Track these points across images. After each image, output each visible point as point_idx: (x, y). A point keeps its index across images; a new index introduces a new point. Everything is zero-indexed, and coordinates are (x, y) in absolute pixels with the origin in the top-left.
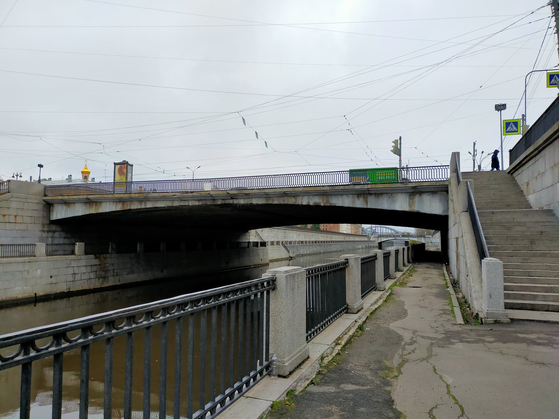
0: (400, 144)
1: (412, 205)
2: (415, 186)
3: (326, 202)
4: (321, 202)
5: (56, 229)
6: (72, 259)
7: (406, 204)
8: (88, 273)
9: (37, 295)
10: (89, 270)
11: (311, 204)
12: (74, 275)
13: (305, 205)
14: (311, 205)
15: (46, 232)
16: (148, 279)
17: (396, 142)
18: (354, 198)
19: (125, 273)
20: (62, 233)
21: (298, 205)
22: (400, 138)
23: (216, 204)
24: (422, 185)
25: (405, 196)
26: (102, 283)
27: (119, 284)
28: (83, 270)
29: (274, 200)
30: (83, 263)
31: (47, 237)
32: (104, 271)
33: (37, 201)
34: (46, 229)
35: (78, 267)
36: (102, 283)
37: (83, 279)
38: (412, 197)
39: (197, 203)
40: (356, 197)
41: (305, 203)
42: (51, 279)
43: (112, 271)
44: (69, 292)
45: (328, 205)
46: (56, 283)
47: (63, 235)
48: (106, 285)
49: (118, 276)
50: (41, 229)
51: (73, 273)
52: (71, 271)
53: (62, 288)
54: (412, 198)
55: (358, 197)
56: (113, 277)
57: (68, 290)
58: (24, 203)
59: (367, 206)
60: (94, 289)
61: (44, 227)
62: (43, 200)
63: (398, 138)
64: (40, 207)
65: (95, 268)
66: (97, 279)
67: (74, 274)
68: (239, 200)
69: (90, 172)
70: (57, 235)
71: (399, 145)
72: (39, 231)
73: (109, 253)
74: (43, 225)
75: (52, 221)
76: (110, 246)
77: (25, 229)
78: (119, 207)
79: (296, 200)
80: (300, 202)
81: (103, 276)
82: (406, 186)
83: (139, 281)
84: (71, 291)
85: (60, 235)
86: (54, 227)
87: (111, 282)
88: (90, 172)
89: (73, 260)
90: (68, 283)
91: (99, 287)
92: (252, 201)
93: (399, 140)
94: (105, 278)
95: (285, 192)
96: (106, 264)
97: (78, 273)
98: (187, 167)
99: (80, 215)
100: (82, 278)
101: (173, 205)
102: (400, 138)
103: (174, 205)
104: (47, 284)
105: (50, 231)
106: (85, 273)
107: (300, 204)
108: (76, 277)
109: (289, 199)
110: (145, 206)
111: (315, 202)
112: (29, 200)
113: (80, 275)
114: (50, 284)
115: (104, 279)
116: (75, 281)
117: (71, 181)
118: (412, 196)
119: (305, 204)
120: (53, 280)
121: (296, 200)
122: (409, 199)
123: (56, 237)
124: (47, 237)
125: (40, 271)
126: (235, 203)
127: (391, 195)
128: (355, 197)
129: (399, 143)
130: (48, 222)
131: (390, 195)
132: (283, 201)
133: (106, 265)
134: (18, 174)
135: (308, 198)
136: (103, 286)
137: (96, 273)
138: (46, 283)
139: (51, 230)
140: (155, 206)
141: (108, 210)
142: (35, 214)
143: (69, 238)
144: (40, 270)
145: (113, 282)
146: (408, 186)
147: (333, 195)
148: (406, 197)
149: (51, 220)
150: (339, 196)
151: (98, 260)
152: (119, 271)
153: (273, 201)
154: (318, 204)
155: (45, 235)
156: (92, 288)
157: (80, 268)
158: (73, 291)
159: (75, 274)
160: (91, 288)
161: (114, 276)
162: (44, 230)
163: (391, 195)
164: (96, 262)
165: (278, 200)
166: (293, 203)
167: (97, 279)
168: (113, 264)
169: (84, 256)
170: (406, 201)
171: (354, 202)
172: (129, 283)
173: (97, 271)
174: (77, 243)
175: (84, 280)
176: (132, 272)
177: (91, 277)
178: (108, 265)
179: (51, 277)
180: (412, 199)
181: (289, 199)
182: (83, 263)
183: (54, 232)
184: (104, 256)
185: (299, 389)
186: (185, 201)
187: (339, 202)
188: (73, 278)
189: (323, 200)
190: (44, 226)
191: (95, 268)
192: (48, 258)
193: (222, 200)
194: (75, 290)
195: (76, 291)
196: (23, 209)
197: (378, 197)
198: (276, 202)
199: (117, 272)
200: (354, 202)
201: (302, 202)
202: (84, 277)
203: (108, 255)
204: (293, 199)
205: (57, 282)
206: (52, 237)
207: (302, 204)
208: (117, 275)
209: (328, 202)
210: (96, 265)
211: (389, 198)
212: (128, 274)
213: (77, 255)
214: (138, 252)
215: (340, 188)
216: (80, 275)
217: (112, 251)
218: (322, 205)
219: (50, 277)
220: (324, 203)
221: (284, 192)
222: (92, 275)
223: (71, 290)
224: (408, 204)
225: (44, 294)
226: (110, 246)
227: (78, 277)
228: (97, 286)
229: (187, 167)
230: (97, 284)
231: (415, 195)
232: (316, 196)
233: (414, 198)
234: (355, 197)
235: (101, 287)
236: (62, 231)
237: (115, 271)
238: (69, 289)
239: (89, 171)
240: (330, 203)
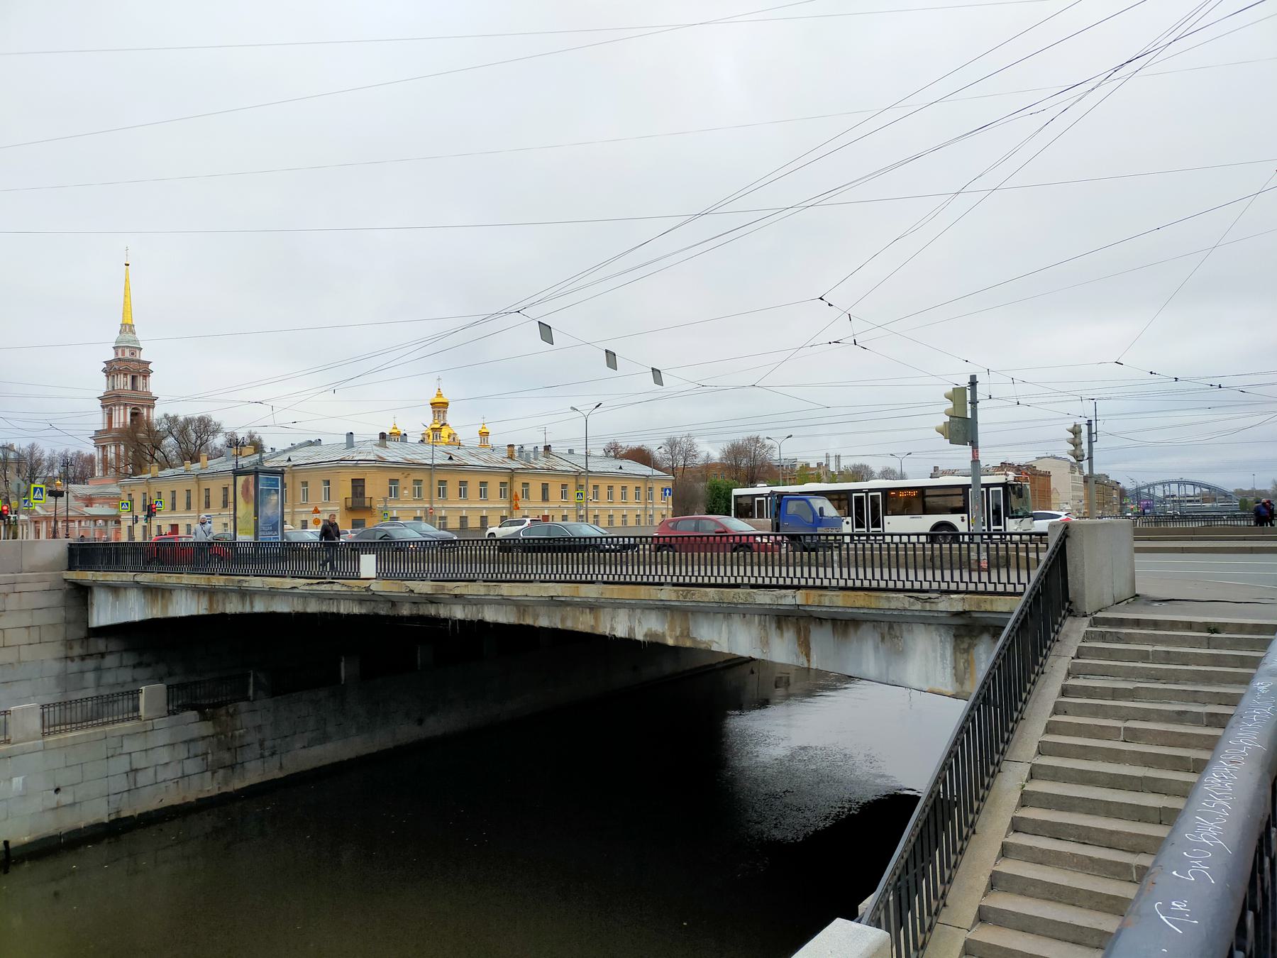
0: (974, 402)
1: (967, 676)
2: (961, 610)
3: (682, 635)
4: (667, 633)
5: (107, 647)
6: (124, 732)
7: (944, 668)
8: (179, 763)
9: (11, 846)
10: (182, 752)
11: (640, 636)
12: (131, 775)
13: (621, 638)
14: (639, 641)
15: (76, 659)
16: (352, 755)
17: (957, 395)
18: (765, 626)
19: (298, 745)
20: (125, 655)
21: (603, 638)
22: (973, 383)
23: (400, 615)
24: (989, 609)
25: (940, 636)
26: (226, 781)
27: (281, 775)
28: (163, 756)
29: (538, 616)
30: (162, 738)
31: (82, 672)
32: (229, 749)
33: (46, 586)
34: (77, 650)
35: (146, 750)
36: (226, 781)
37: (162, 780)
38: (963, 642)
39: (356, 609)
40: (774, 626)
41: (621, 632)
42: (57, 797)
43: (257, 746)
44: (119, 821)
45: (688, 644)
46: (73, 804)
47: (130, 659)
48: (237, 784)
49: (276, 758)
50: (62, 654)
51: (128, 769)
52: (122, 764)
53: (97, 812)
54: (965, 646)
55: (779, 627)
56: (259, 762)
57: (113, 817)
58: (7, 595)
59: (809, 661)
60: (198, 800)
61: (71, 648)
62: (65, 579)
63: (965, 382)
64: (57, 598)
65: (200, 747)
66: (209, 774)
67: (132, 770)
68: (452, 606)
69: (447, 404)
70: (110, 661)
71: (969, 406)
72: (56, 659)
73: (248, 699)
74: (68, 643)
75: (92, 628)
76: (251, 680)
77: (10, 661)
78: (204, 607)
79: (596, 619)
80: (609, 627)
81: (228, 763)
82: (928, 607)
83: (345, 758)
84: (124, 818)
85: (121, 662)
86: (101, 644)
87: (254, 774)
88: (447, 404)
89: (128, 735)
90: (112, 798)
91: (215, 792)
92: (482, 613)
93: (968, 392)
94: (233, 768)
95: (554, 598)
96: (237, 730)
97: (146, 768)
98: (572, 408)
99: (137, 619)
100: (160, 778)
101: (305, 608)
102: (973, 383)
103: (309, 610)
104: (43, 811)
105: (91, 655)
106: (167, 763)
107: (607, 634)
108: (138, 779)
109: (578, 614)
110: (252, 607)
111: (650, 630)
112: (19, 588)
113: (151, 772)
114: (53, 809)
115: (230, 771)
116: (135, 790)
117: (353, 447)
118: (967, 640)
119: (623, 636)
120: (65, 798)
121: (596, 619)
122: (954, 648)
123: (110, 668)
124: (82, 672)
125: (21, 781)
126: (442, 616)
127: (891, 627)
128: (767, 624)
129: (969, 398)
130: (82, 633)
131: (887, 629)
132: (563, 620)
133: (237, 733)
134: (239, 441)
135: (629, 616)
136: (230, 789)
137: (203, 759)
138: (41, 810)
139: (93, 652)
140: (271, 610)
141: (183, 613)
142: (42, 618)
143: (148, 665)
144: (21, 779)
145: (259, 775)
146: (934, 607)
147: (699, 612)
148: (941, 641)
149: (90, 626)
150: (719, 615)
151: (210, 723)
152: (279, 741)
153: (536, 617)
154: (660, 641)
155: (74, 667)
156: (193, 800)
157: (150, 752)
158: (132, 816)
159: (136, 770)
160: (188, 800)
161: (262, 756)
162: (70, 655)
163: (891, 627)
164: (206, 728)
165: (549, 617)
166: (589, 630)
167: (209, 774)
168: (259, 728)
169: (167, 718)
170: (943, 656)
171: (765, 643)
172: (315, 770)
173: (207, 753)
174: (143, 688)
175: (164, 781)
176: (324, 739)
177: (187, 772)
178: (241, 731)
179: (57, 790)
180: (967, 651)
181: (578, 614)
182: (162, 738)
183: (102, 655)
184: (231, 710)
185: (1070, 667)
186: (331, 601)
187: (720, 639)
188: (129, 783)
189: (672, 629)
190: (70, 644)
191: (200, 747)
192: (47, 742)
193: (412, 604)
194: (138, 812)
195: (140, 815)
196: (5, 611)
197: (845, 633)
198: (543, 622)
199: (274, 747)
200: (765, 643)
201: (613, 628)
202: (169, 773)
203: (243, 706)
204: (588, 616)
205: (76, 801)
206: (98, 669)
207: (614, 635)
208: (273, 754)
209: (686, 634)
210: (204, 738)
211: (883, 639)
212: (309, 746)
213: (143, 719)
214: (343, 683)
215: (706, 594)
216: (151, 772)
217: (255, 692)
218: (670, 642)
219: (53, 792)
220: (677, 638)
221: (552, 597)
222: (192, 766)
223: (124, 814)
224: (949, 671)
225: (34, 840)
226: (251, 680)
227: (142, 779)
228: (208, 791)
229: (572, 408)
230: (209, 787)
231: (976, 637)
232: (654, 612)
233: (971, 646)
234: (767, 624)
235: (222, 793)
236: (126, 650)
237: (268, 744)
238: (118, 812)
239: (446, 401)
240: (694, 639)
